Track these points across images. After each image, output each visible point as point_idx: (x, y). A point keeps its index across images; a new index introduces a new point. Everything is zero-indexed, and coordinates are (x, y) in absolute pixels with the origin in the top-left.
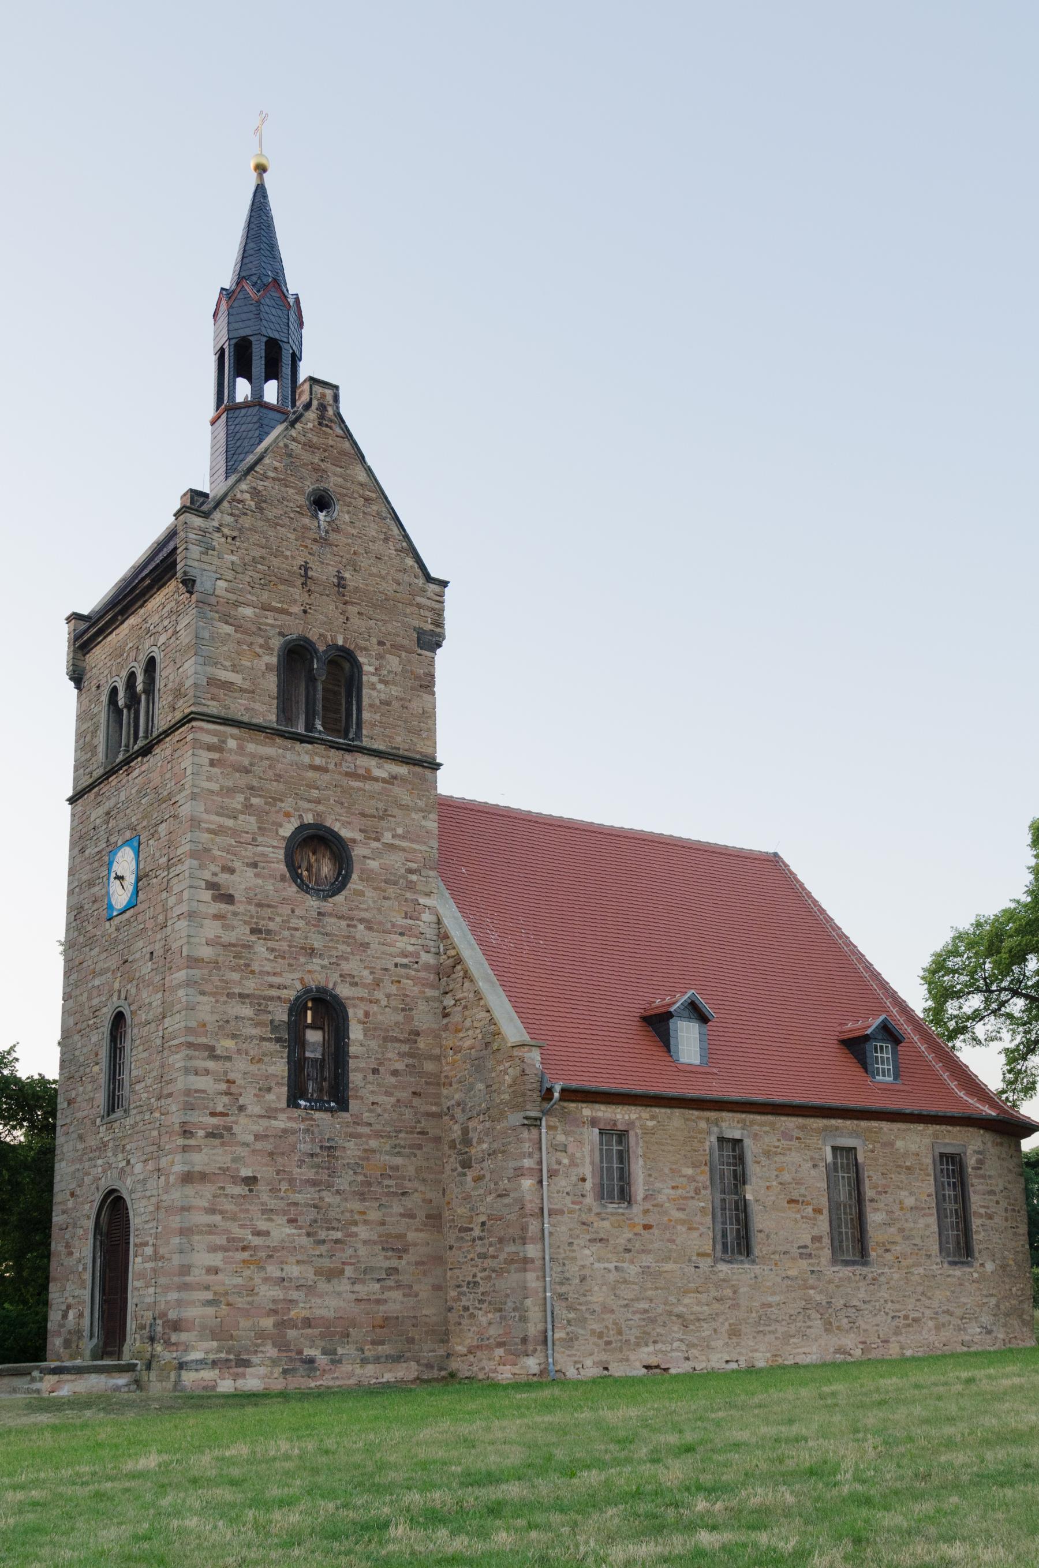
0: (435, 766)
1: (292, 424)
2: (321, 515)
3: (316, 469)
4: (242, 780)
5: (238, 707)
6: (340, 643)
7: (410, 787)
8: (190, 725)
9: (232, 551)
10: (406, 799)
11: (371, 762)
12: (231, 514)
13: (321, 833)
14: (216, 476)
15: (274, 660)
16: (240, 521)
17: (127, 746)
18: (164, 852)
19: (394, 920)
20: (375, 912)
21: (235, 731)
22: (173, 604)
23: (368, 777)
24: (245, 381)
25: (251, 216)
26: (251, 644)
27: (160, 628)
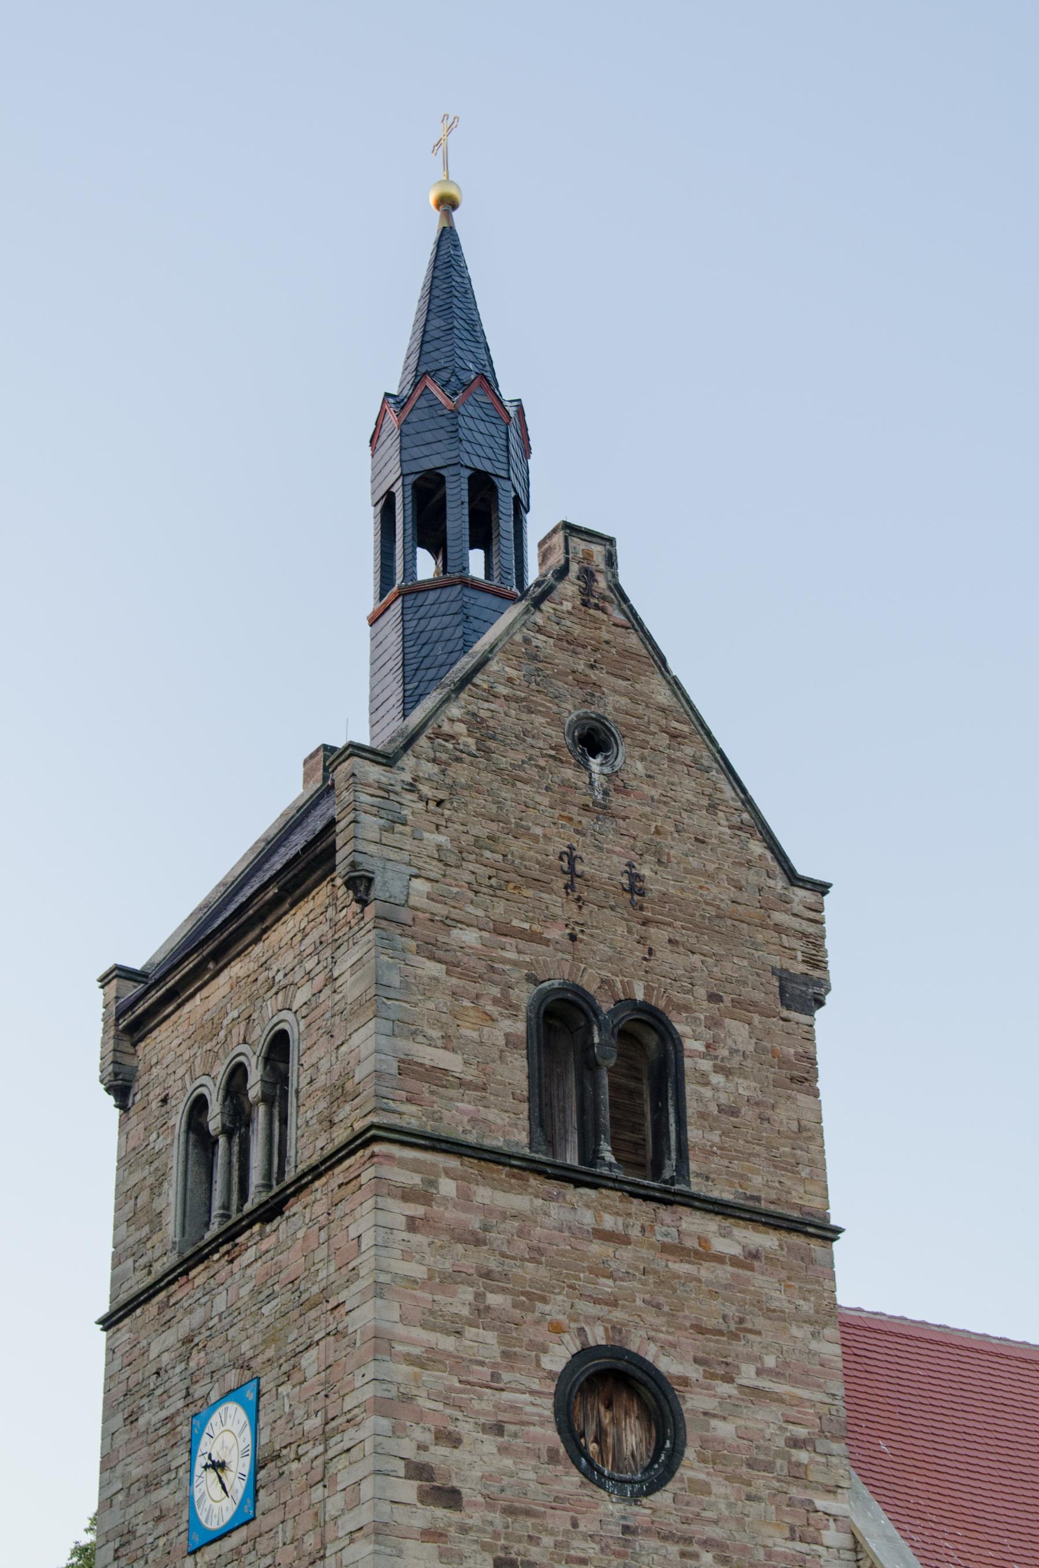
0: (829, 1234)
1: (537, 603)
2: (595, 763)
3: (582, 682)
4: (470, 1259)
5: (457, 1117)
6: (640, 995)
7: (784, 1274)
8: (368, 1152)
9: (437, 826)
10: (779, 1299)
11: (708, 1225)
12: (434, 760)
13: (621, 1365)
14: (381, 711)
15: (520, 1027)
16: (450, 772)
17: (226, 1206)
18: (314, 1406)
19: (769, 1542)
20: (733, 1525)
21: (453, 1162)
22: (325, 928)
23: (703, 1254)
24: (425, 551)
25: (433, 278)
26: (478, 996)
27: (299, 973)
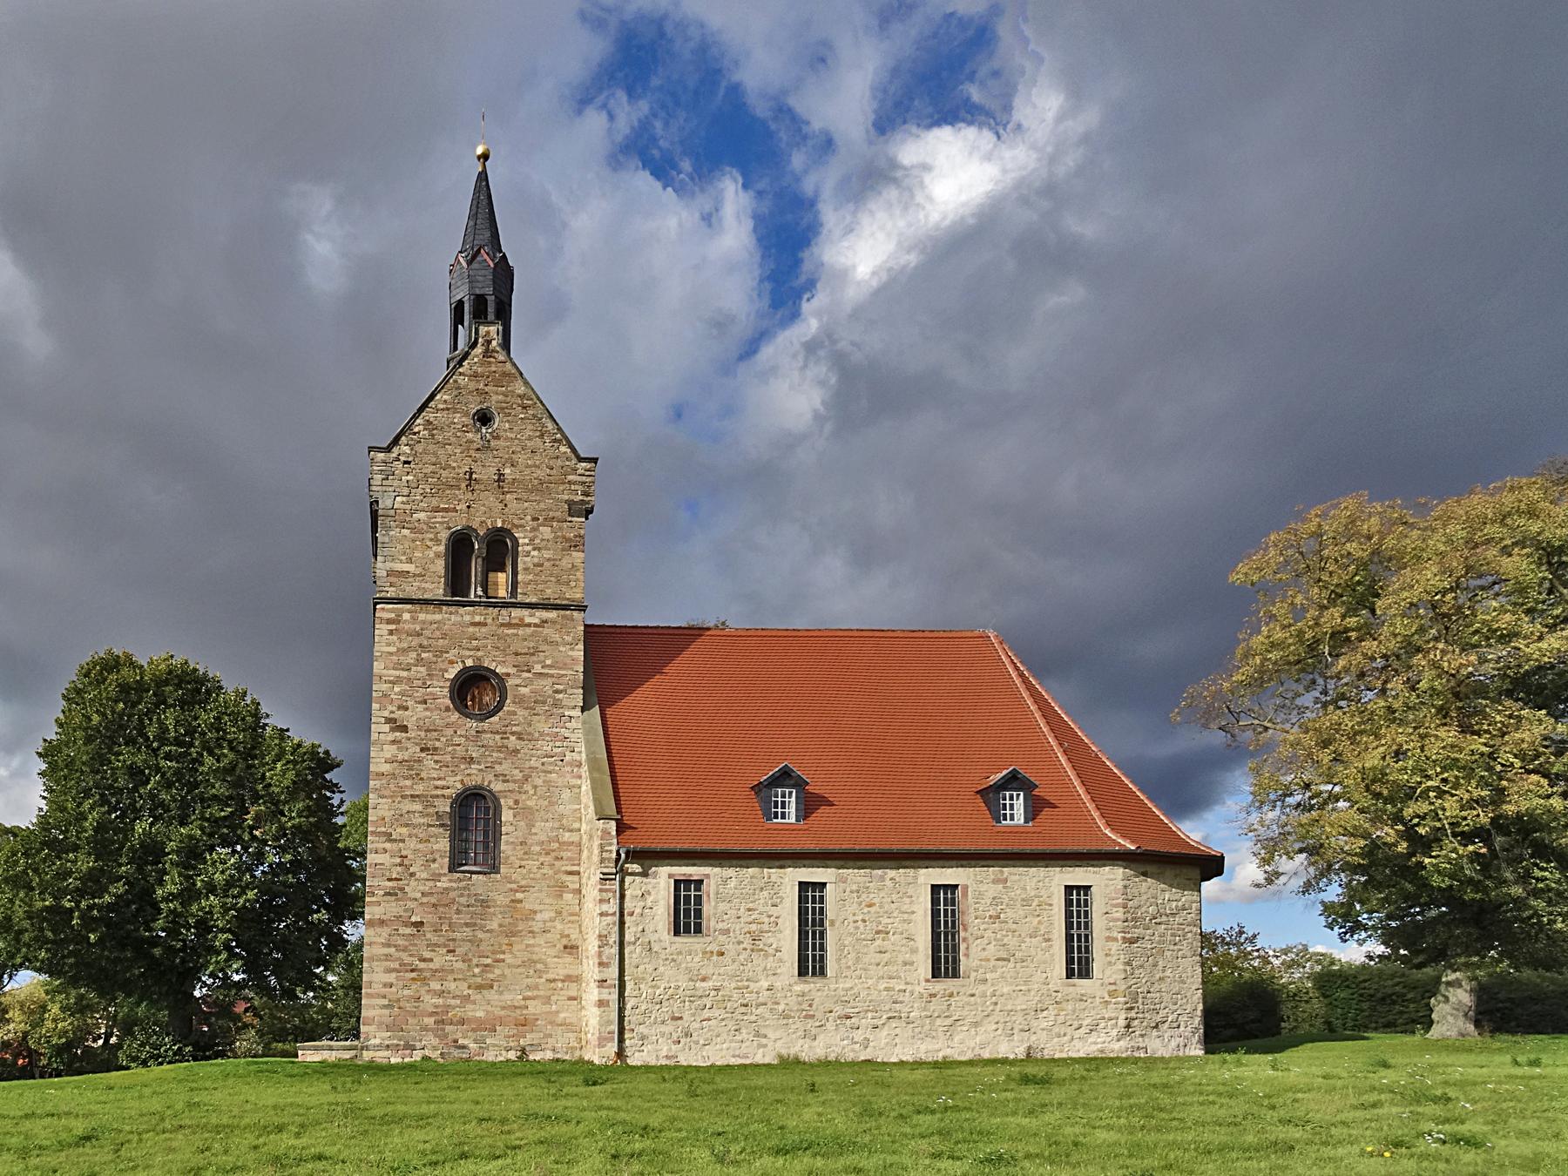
4: (415, 642)
5: (412, 589)
15: (442, 548)
21: (409, 606)
